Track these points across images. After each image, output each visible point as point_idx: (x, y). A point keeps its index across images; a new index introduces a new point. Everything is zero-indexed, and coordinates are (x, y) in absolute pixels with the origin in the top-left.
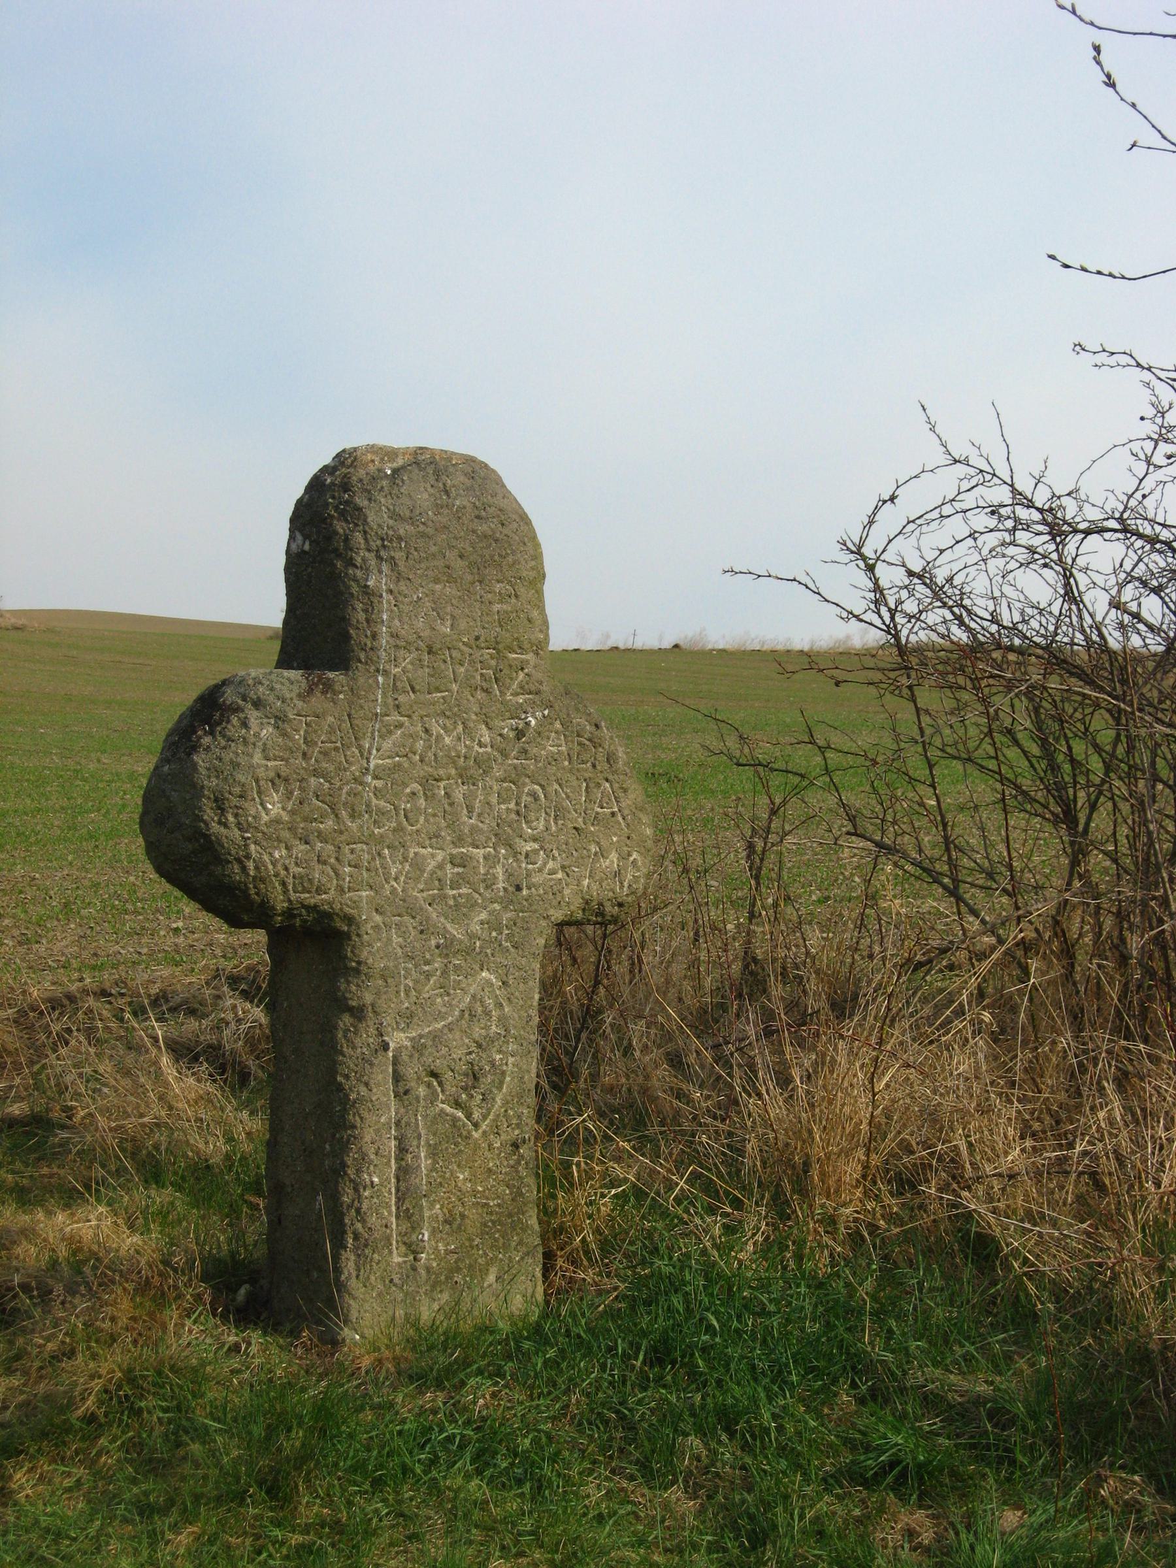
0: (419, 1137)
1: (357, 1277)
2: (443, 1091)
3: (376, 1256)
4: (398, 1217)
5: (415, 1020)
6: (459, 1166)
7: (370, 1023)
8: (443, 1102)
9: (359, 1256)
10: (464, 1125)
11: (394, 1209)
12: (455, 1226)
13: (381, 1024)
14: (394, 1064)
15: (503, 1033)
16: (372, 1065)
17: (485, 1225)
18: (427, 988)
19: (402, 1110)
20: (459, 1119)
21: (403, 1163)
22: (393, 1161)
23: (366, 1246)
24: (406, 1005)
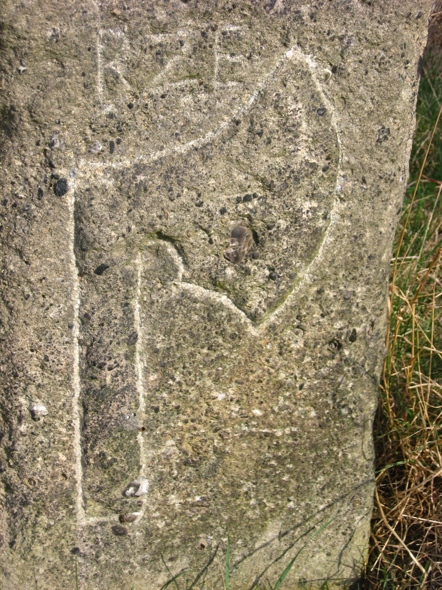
0: (133, 338)
1: (12, 544)
2: (185, 263)
3: (44, 519)
4: (85, 464)
5: (131, 136)
6: (216, 380)
7: (30, 142)
8: (185, 279)
9: (15, 515)
10: (230, 318)
11: (78, 451)
12: (204, 468)
13: (51, 145)
14: (77, 219)
15: (322, 163)
16: (30, 218)
17: (265, 464)
18: (157, 78)
19: (95, 298)
20: (221, 307)
21: (96, 384)
22: (76, 379)
23: (25, 503)
24: (110, 108)
